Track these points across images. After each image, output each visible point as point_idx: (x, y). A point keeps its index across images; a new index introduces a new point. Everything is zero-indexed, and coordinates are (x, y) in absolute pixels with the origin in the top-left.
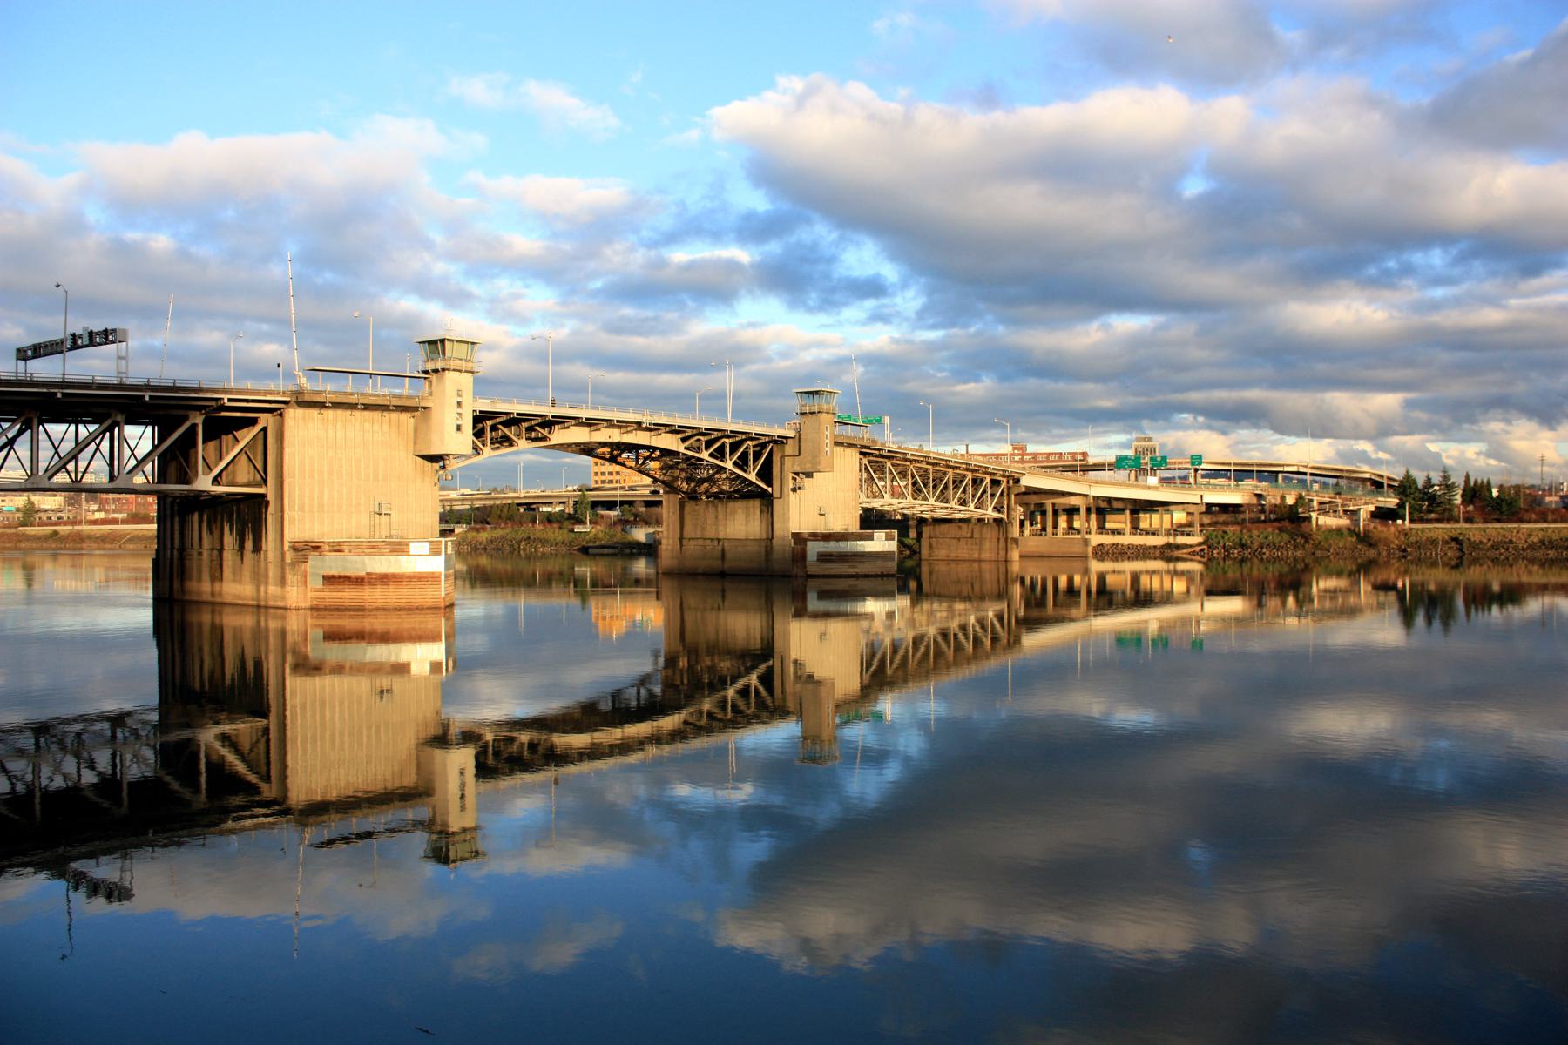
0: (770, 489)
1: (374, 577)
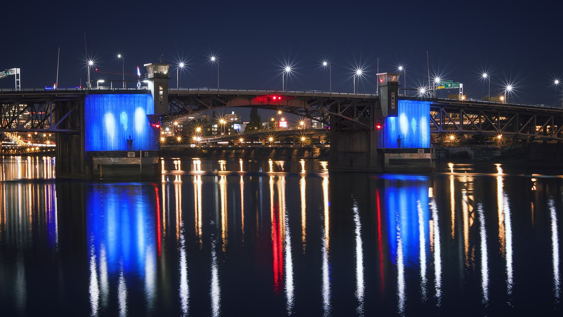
0: (368, 126)
1: (114, 166)
